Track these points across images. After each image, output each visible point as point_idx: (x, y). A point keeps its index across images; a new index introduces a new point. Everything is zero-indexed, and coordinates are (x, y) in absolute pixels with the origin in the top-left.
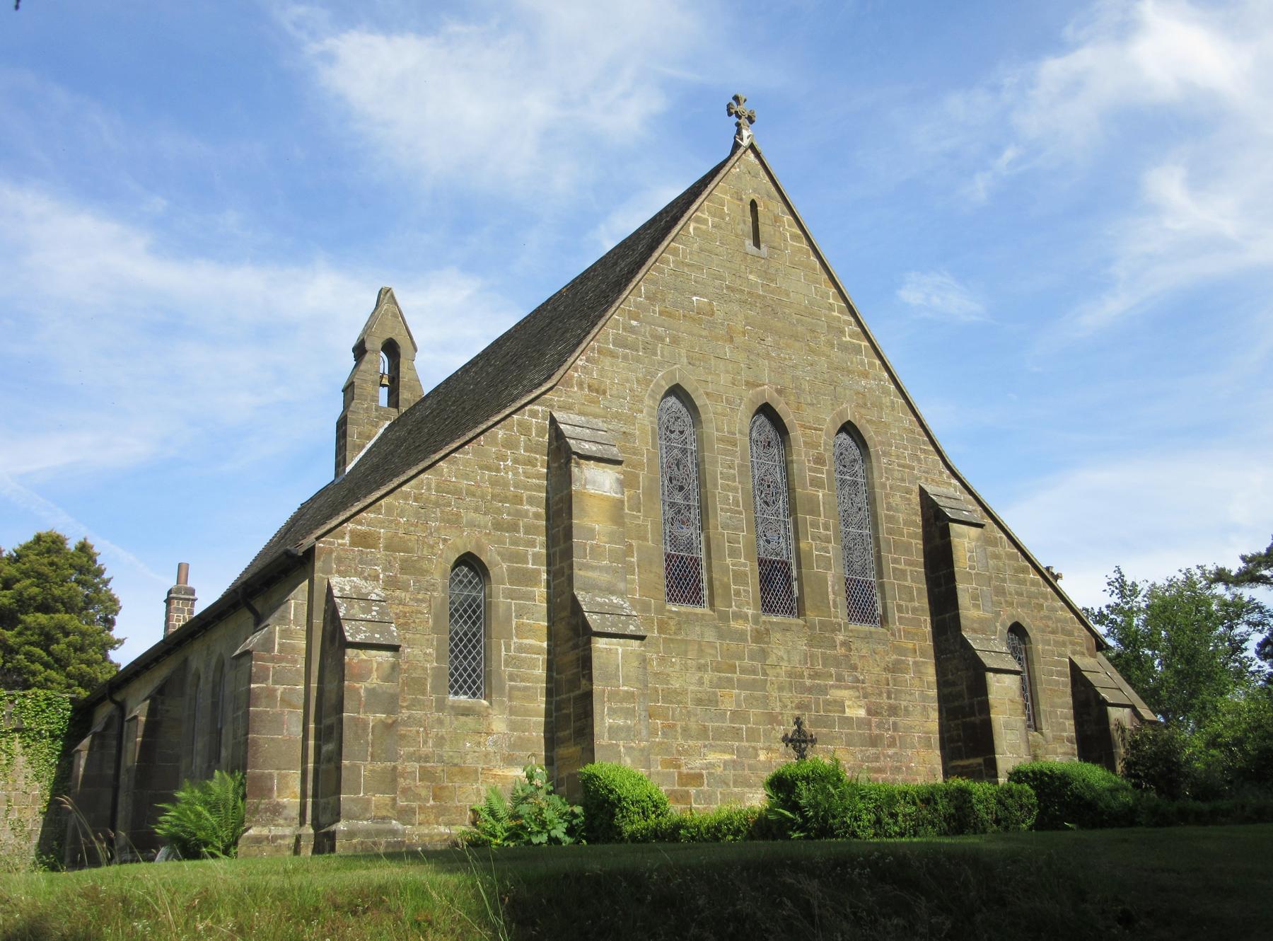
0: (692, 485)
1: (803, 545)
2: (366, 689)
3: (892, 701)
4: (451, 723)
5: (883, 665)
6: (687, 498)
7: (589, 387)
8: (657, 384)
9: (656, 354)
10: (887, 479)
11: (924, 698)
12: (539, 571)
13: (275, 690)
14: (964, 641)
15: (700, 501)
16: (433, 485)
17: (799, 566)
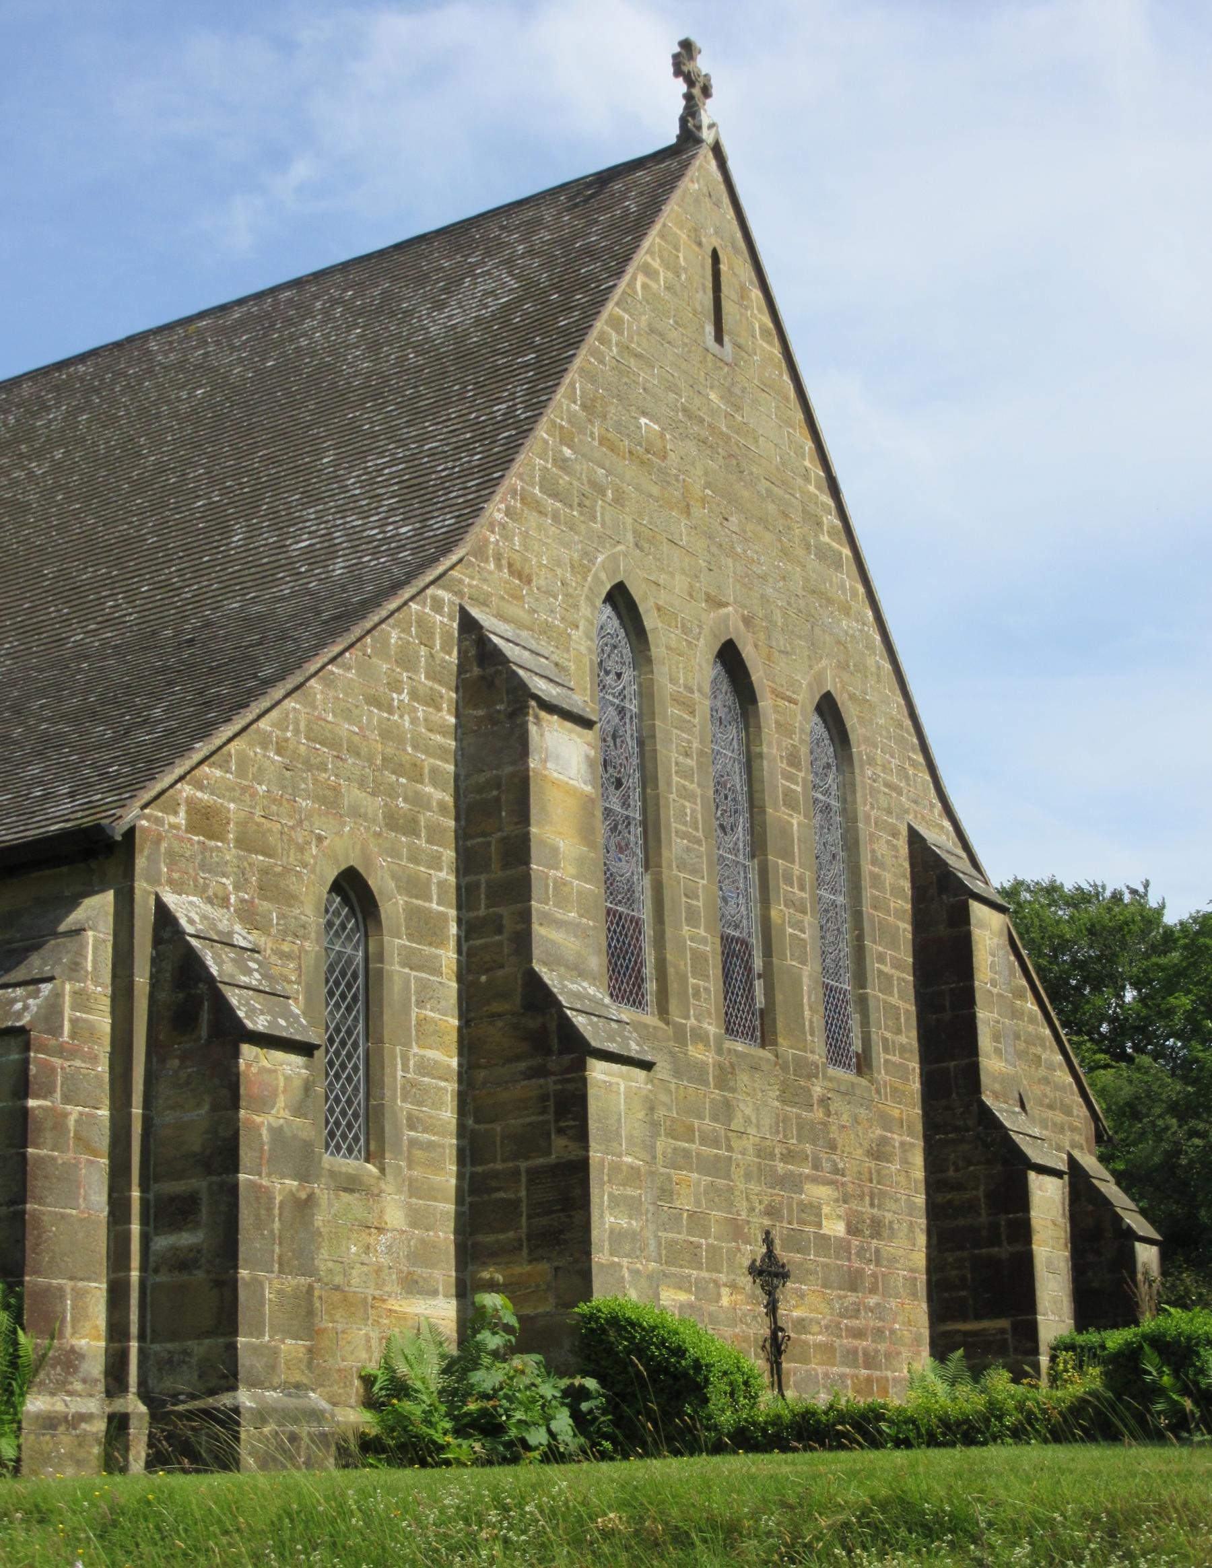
0: (633, 780)
1: (774, 914)
2: (271, 1128)
3: (875, 1211)
4: (330, 1205)
5: (866, 1144)
6: (625, 804)
7: (510, 565)
8: (596, 577)
9: (593, 518)
10: (872, 807)
11: (911, 1206)
12: (443, 917)
13: (65, 1115)
14: (987, 1118)
15: (644, 811)
16: (302, 727)
17: (768, 952)
